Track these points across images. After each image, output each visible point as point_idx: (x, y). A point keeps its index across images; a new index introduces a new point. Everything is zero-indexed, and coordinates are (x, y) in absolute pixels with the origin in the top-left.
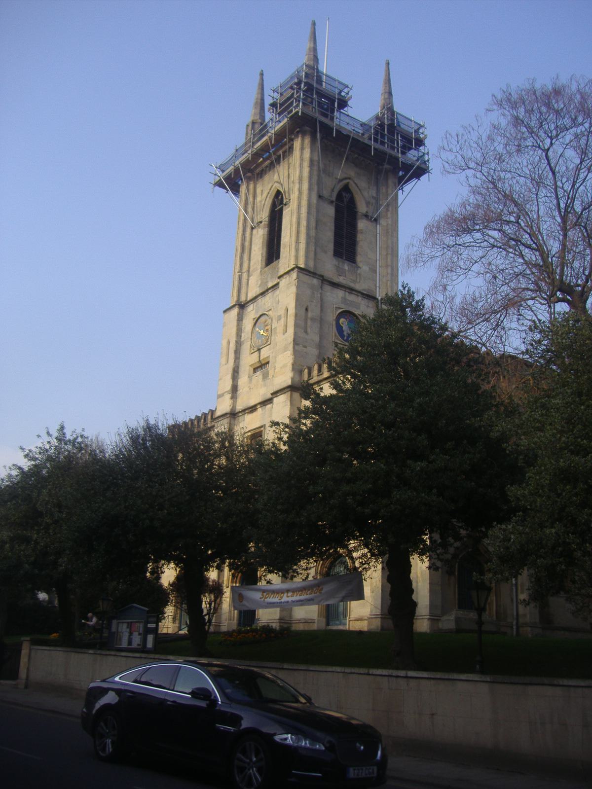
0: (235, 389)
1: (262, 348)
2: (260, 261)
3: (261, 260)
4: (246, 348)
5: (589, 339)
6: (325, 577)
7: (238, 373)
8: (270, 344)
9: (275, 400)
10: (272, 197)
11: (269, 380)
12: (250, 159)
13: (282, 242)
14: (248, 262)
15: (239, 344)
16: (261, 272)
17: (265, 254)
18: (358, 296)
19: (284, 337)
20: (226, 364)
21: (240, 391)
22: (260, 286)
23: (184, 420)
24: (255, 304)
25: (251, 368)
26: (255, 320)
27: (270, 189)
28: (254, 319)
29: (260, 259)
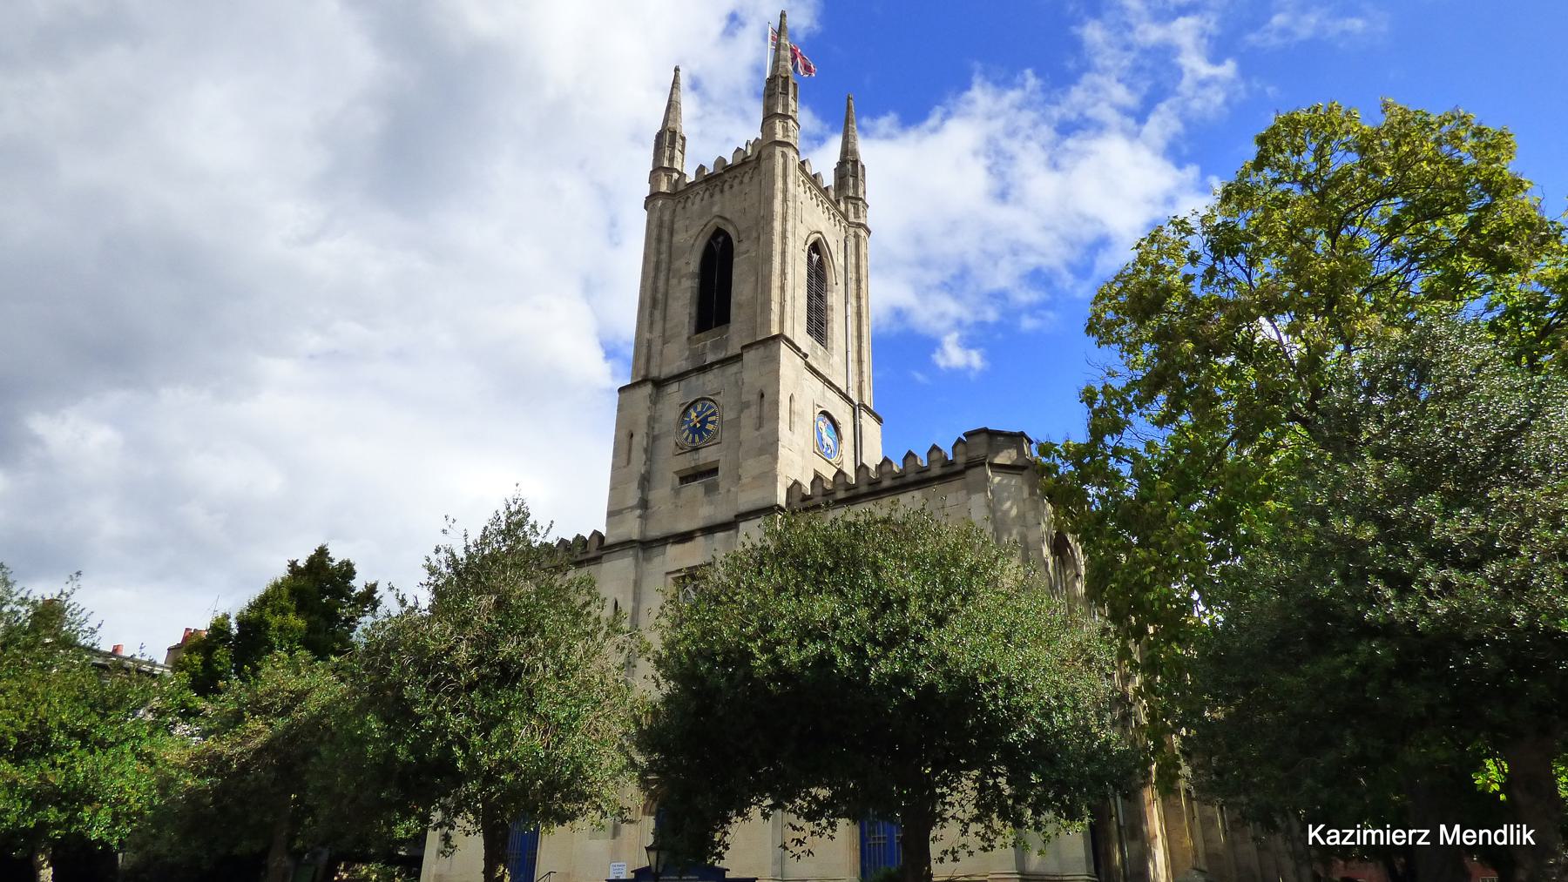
0: (644, 504)
1: (701, 448)
2: (687, 324)
3: (689, 322)
4: (668, 445)
5: (1561, 442)
6: (1012, 158)
7: (648, 481)
8: (718, 443)
9: (742, 526)
10: (708, 237)
11: (720, 496)
12: (1310, 826)
13: (732, 300)
14: (661, 322)
15: (826, 460)
16: (689, 338)
17: (694, 314)
18: (863, 166)
19: (757, 433)
20: (624, 467)
21: (654, 509)
22: (686, 359)
23: (224, 612)
24: (683, 383)
25: (675, 476)
26: (684, 407)
27: (705, 226)
28: (683, 404)
29: (687, 320)
